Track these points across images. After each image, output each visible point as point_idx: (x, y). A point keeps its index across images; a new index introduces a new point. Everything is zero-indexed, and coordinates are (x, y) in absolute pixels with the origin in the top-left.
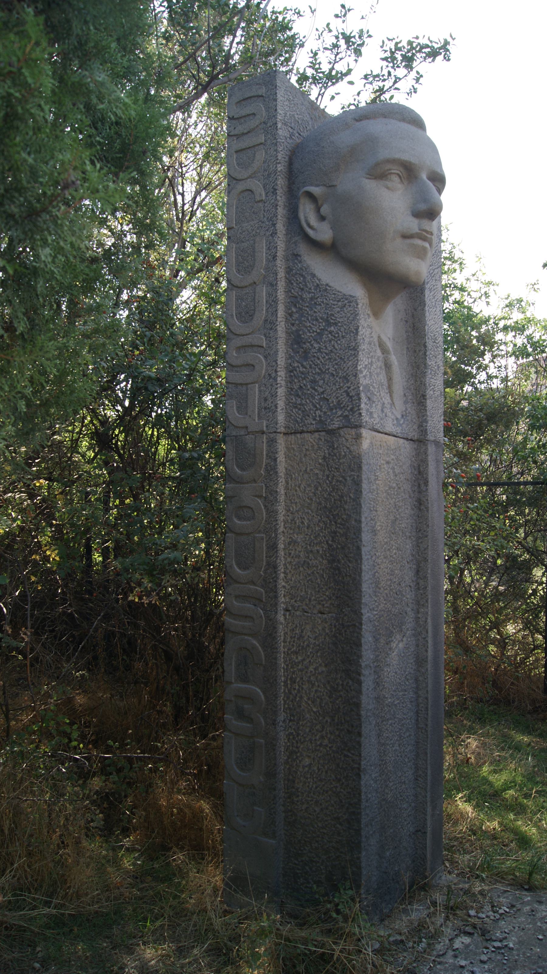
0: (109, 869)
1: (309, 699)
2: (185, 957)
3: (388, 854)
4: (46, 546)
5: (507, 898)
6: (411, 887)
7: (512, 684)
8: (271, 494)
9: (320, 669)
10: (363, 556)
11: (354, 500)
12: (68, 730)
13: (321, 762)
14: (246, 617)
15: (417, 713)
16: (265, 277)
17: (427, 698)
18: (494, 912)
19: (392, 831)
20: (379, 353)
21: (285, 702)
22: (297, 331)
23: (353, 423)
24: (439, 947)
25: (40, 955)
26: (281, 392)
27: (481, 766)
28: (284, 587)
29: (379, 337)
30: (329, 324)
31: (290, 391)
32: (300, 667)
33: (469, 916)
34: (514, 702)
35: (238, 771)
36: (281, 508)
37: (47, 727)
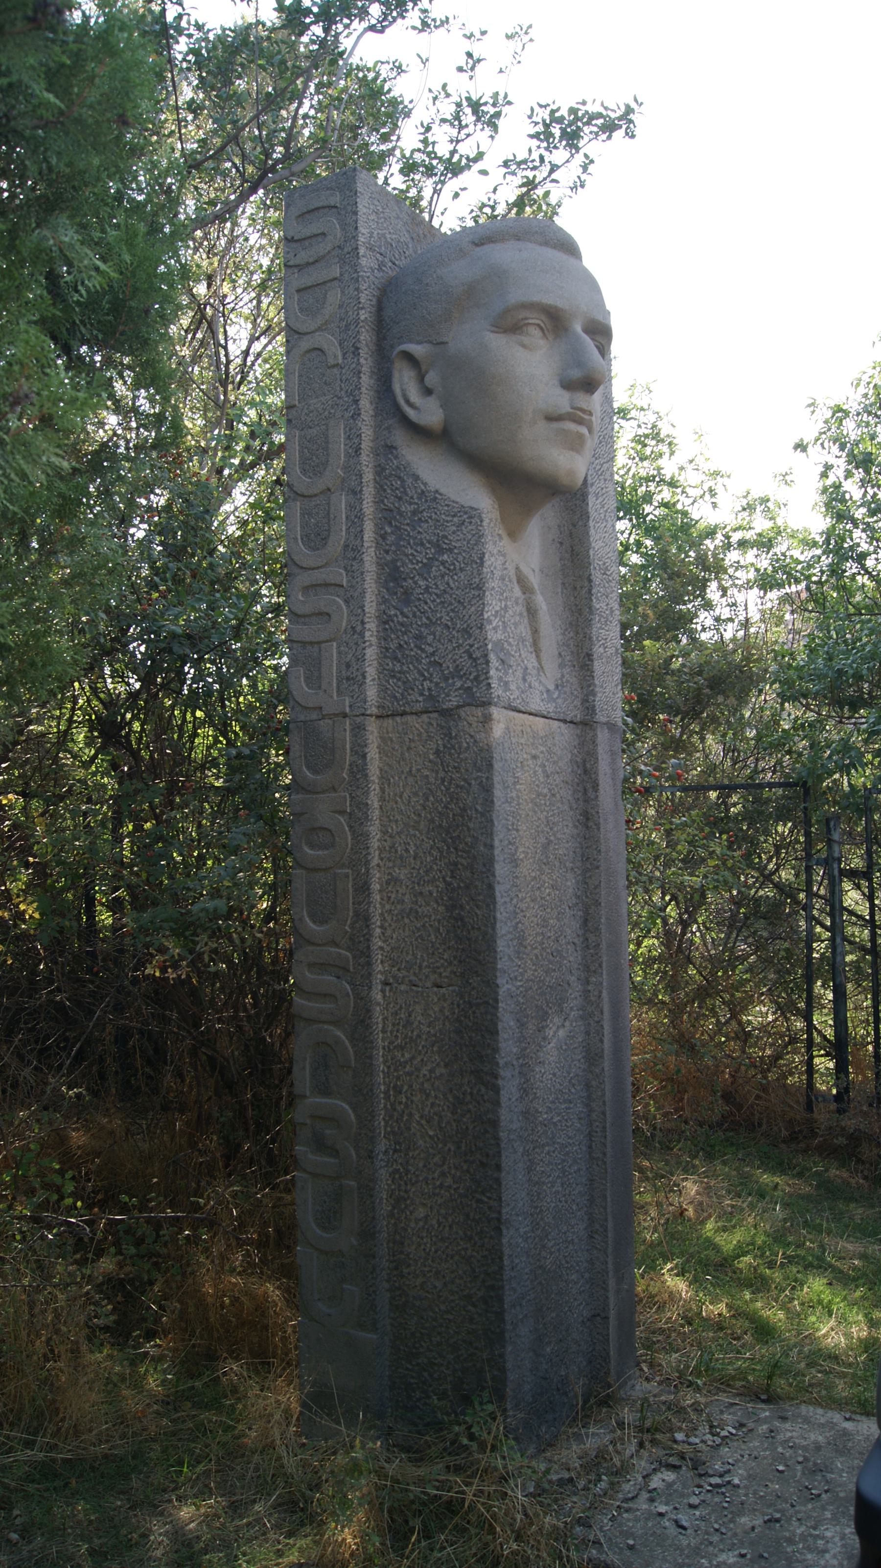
0: (126, 1392)
1: (421, 1117)
2: (241, 1517)
3: (548, 1349)
4: (18, 896)
5: (734, 1414)
6: (585, 1402)
7: (758, 1097)
8: (360, 809)
10: (498, 899)
11: (482, 815)
12: (58, 1180)
14: (325, 995)
16: (343, 480)
17: (604, 1113)
18: (714, 1435)
20: (517, 591)
21: (386, 1122)
22: (394, 561)
23: (478, 697)
24: (628, 1488)
25: (18, 1521)
26: (371, 653)
27: (703, 1222)
28: (381, 948)
29: (517, 568)
30: (441, 551)
31: (385, 652)
34: (760, 1125)
35: (318, 1231)
36: (374, 830)
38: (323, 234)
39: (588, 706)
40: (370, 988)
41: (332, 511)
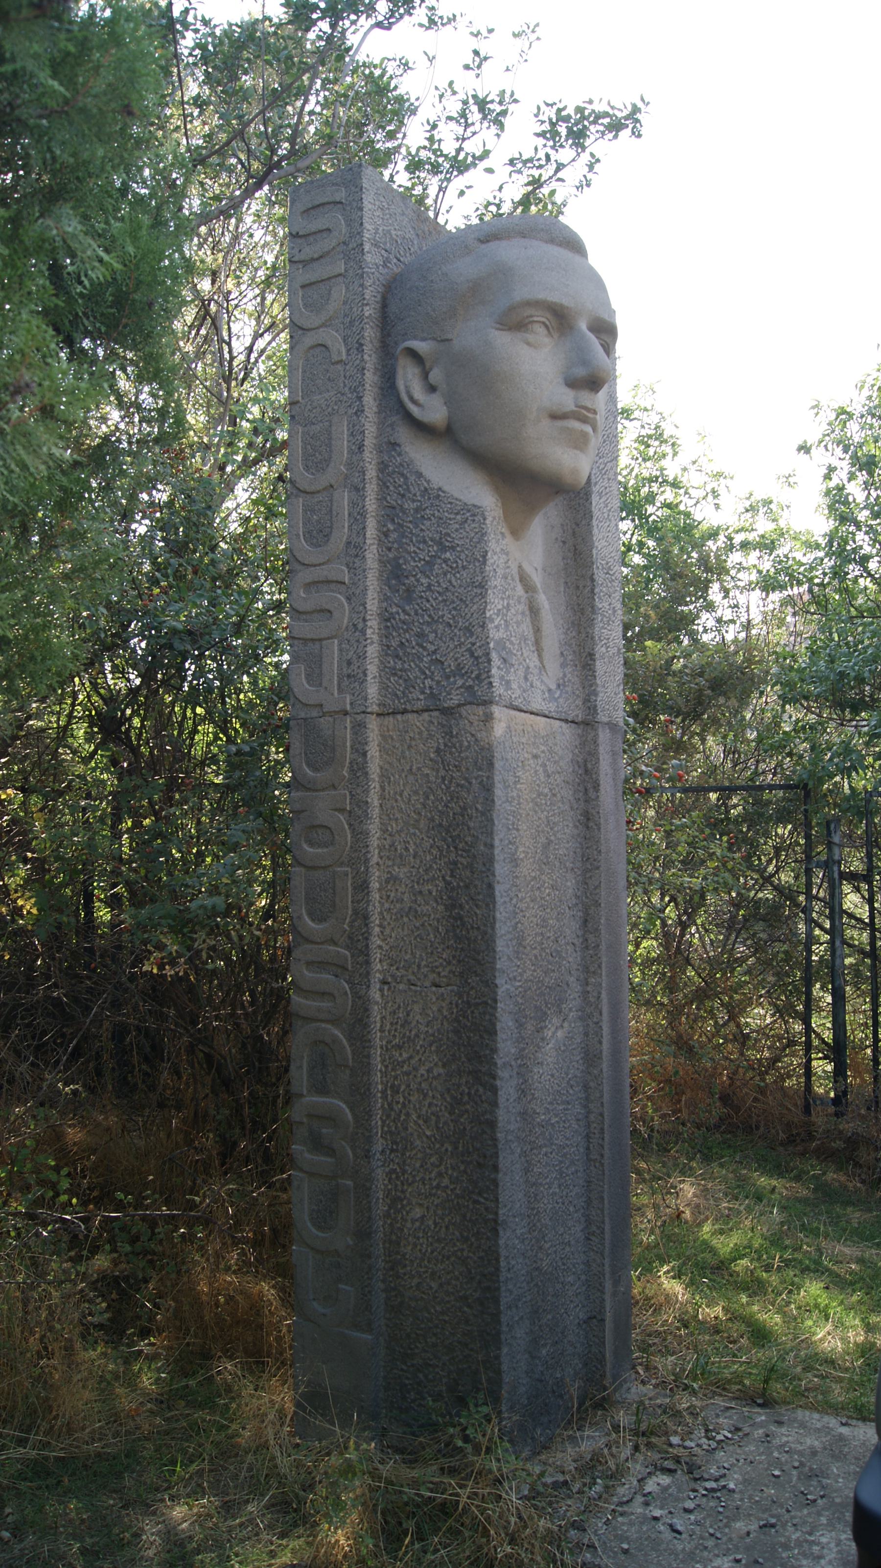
0: (119, 1391)
1: (419, 1117)
2: (234, 1517)
4: (16, 891)
5: (730, 1418)
6: (581, 1405)
7: (756, 1100)
9: (435, 1072)
10: (498, 899)
11: (483, 814)
12: (53, 1177)
13: (440, 1212)
14: (323, 994)
15: (588, 1136)
17: (602, 1115)
19: (549, 1317)
20: (520, 590)
21: (383, 1122)
22: (396, 559)
24: (623, 1491)
25: (10, 1519)
26: (373, 651)
27: (700, 1225)
28: (380, 947)
29: (520, 567)
30: (444, 549)
31: (386, 649)
32: (405, 1068)
33: (671, 1445)
34: (757, 1128)
35: (314, 1230)
36: (374, 828)
37: (20, 1172)
39: (590, 707)
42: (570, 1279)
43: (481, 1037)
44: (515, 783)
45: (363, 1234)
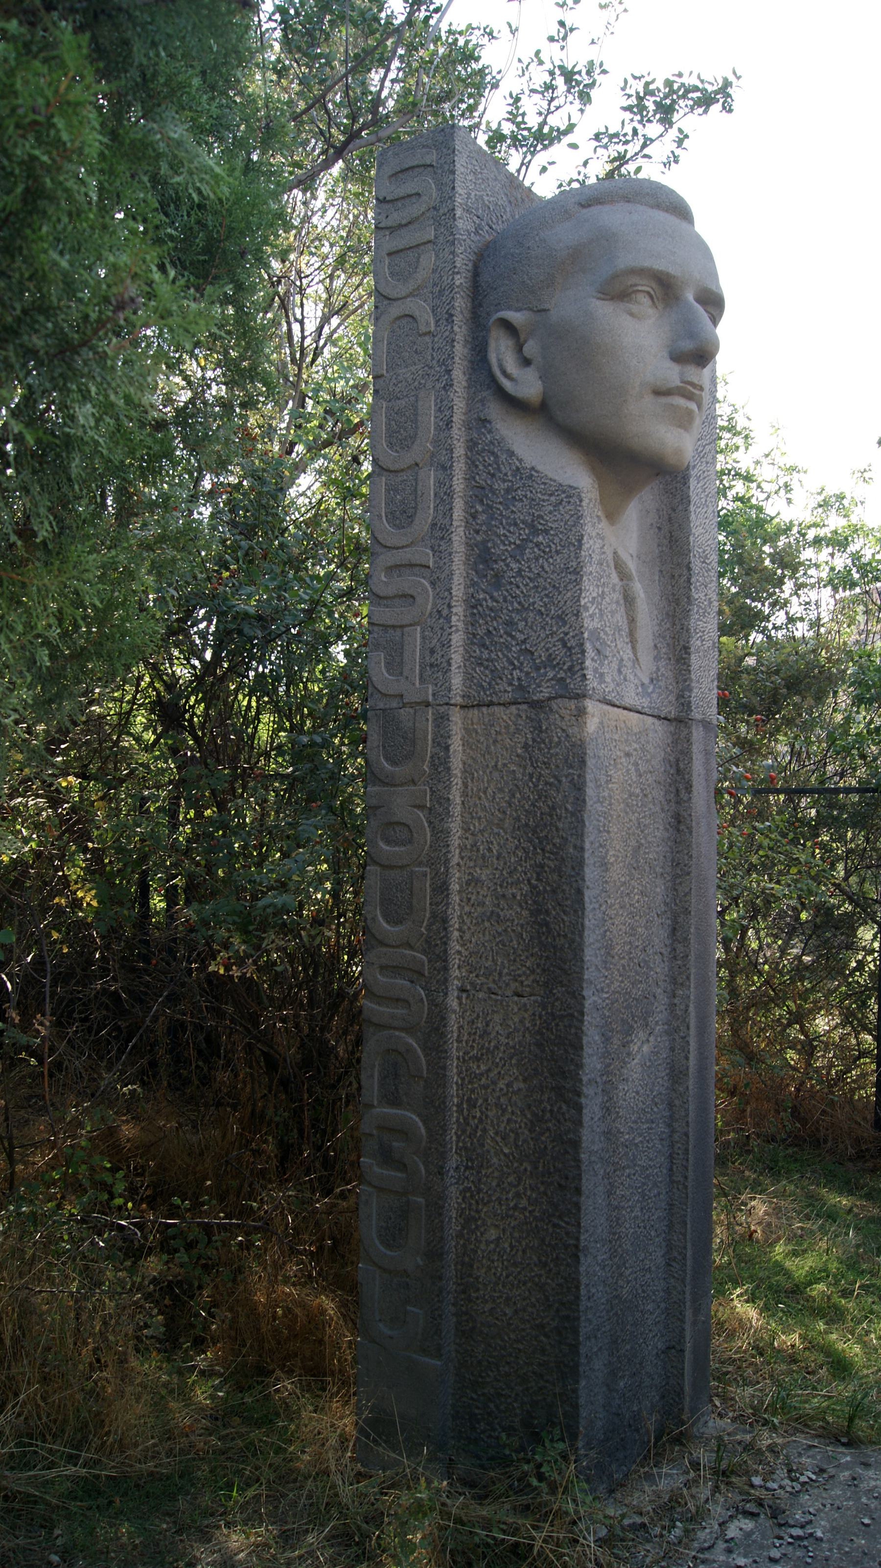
0: (173, 1405)
1: (496, 1133)
5: (813, 1457)
6: (658, 1438)
9: (515, 1086)
11: (573, 814)
12: (109, 1180)
13: (516, 1235)
14: (397, 1000)
16: (433, 455)
17: (686, 1134)
18: (792, 1480)
19: (628, 1347)
20: (615, 578)
21: (458, 1137)
22: (485, 542)
23: (572, 690)
25: (59, 1542)
26: (457, 639)
27: (772, 1245)
28: (459, 952)
30: (536, 532)
31: (471, 637)
33: (752, 1486)
34: (825, 1142)
35: (382, 1248)
36: (455, 826)
37: (75, 1174)
38: (418, 194)
39: (683, 701)
40: (446, 994)
41: (419, 487)
42: (650, 1307)
43: (566, 1051)
44: (607, 782)
45: (434, 1254)
